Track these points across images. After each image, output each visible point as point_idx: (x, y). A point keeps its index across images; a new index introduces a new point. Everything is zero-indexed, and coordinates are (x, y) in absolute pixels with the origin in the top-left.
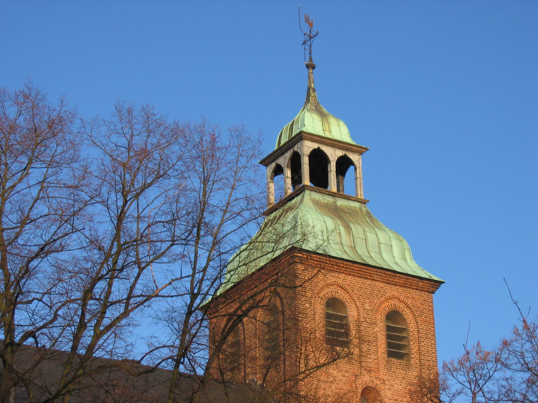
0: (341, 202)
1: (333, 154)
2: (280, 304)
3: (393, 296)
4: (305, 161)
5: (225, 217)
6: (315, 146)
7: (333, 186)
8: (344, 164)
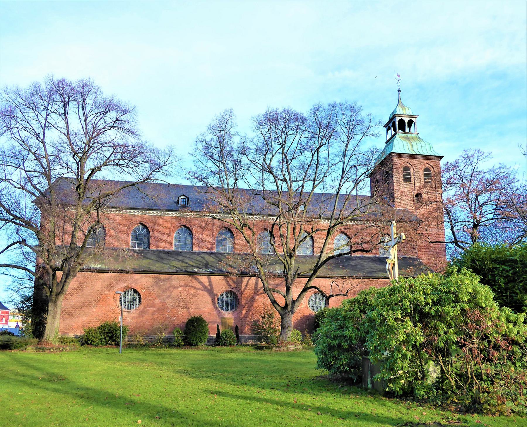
0: (409, 135)
1: (406, 120)
2: (292, 400)
3: (425, 163)
4: (397, 123)
5: (315, 184)
6: (400, 118)
7: (407, 130)
8: (410, 122)
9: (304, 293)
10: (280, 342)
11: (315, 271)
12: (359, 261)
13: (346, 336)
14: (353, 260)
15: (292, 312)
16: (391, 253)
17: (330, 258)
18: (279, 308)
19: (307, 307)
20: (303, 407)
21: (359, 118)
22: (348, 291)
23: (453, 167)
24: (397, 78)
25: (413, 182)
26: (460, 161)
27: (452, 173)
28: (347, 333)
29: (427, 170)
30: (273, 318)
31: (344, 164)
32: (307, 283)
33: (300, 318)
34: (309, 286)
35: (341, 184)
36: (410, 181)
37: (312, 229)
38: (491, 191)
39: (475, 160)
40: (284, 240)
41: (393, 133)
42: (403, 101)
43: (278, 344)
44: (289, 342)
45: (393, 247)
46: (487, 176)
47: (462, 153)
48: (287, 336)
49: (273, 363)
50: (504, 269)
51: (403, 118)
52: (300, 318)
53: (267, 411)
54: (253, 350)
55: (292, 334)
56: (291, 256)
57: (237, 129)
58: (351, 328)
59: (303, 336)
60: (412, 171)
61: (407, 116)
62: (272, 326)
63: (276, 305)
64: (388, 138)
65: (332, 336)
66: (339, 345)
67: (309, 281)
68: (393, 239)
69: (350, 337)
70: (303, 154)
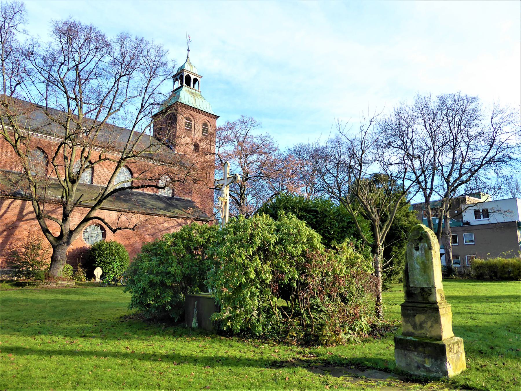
0: (193, 91)
1: (193, 77)
5: (111, 112)
6: (187, 74)
8: (195, 80)
9: (85, 224)
10: (48, 276)
11: (100, 201)
12: (141, 197)
13: (170, 272)
14: (135, 195)
15: (68, 243)
16: (224, 191)
17: (115, 191)
18: (52, 239)
19: (85, 239)
20: (154, 357)
21: (163, 60)
22: (136, 225)
23: (231, 127)
24: (188, 38)
25: (193, 132)
26: (237, 124)
27: (229, 132)
28: (172, 269)
29: (205, 124)
30: (39, 248)
31: (143, 99)
32: (89, 213)
33: (72, 251)
34: (91, 216)
35: (140, 118)
36: (191, 131)
37: (100, 156)
38: (261, 153)
39: (249, 126)
40: (68, 163)
41: (180, 85)
42: (191, 59)
43: (46, 279)
44: (60, 278)
45: (226, 186)
46: (255, 140)
47: (240, 117)
48: (59, 271)
49: (49, 303)
50: (309, 218)
51: (190, 75)
52: (72, 251)
53: (114, 369)
54: (10, 287)
55: (63, 269)
56: (73, 182)
57: (27, 27)
58: (174, 264)
59: (75, 270)
60: (193, 122)
61: (194, 74)
62: (38, 259)
63: (48, 234)
64: (175, 89)
65: (155, 272)
66: (163, 284)
67: (91, 211)
68: (226, 179)
69: (175, 273)
70: (98, 78)
